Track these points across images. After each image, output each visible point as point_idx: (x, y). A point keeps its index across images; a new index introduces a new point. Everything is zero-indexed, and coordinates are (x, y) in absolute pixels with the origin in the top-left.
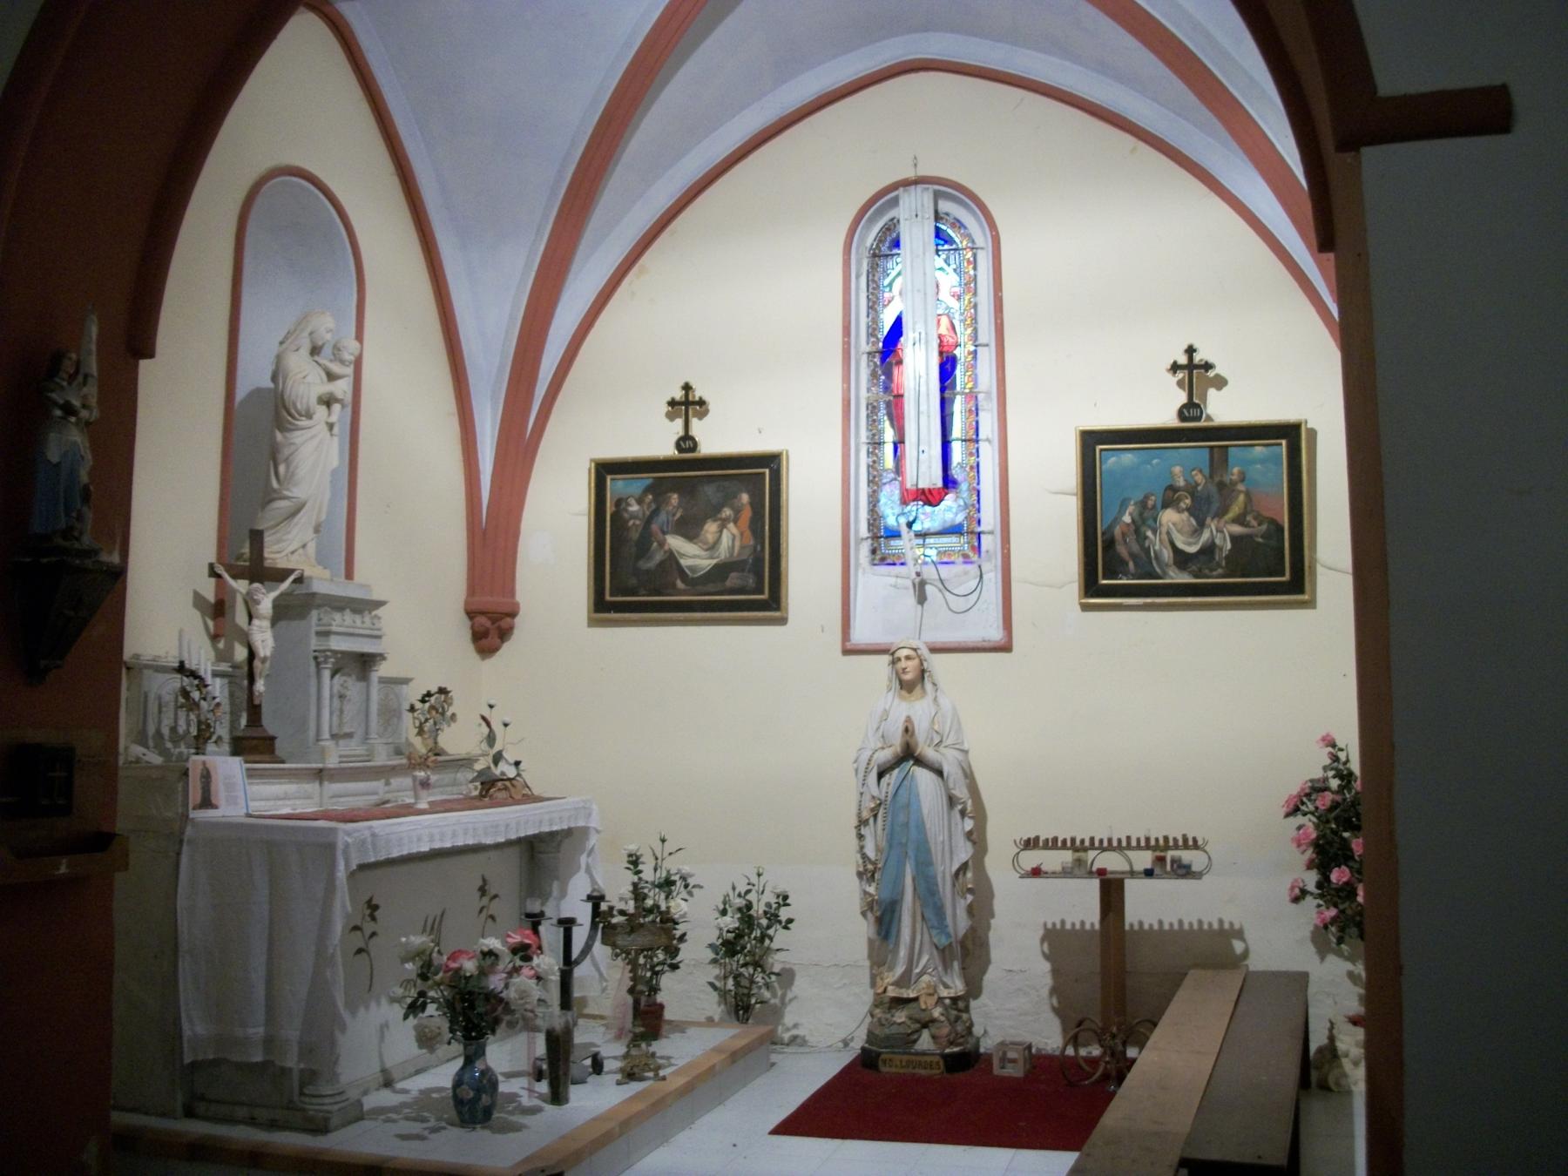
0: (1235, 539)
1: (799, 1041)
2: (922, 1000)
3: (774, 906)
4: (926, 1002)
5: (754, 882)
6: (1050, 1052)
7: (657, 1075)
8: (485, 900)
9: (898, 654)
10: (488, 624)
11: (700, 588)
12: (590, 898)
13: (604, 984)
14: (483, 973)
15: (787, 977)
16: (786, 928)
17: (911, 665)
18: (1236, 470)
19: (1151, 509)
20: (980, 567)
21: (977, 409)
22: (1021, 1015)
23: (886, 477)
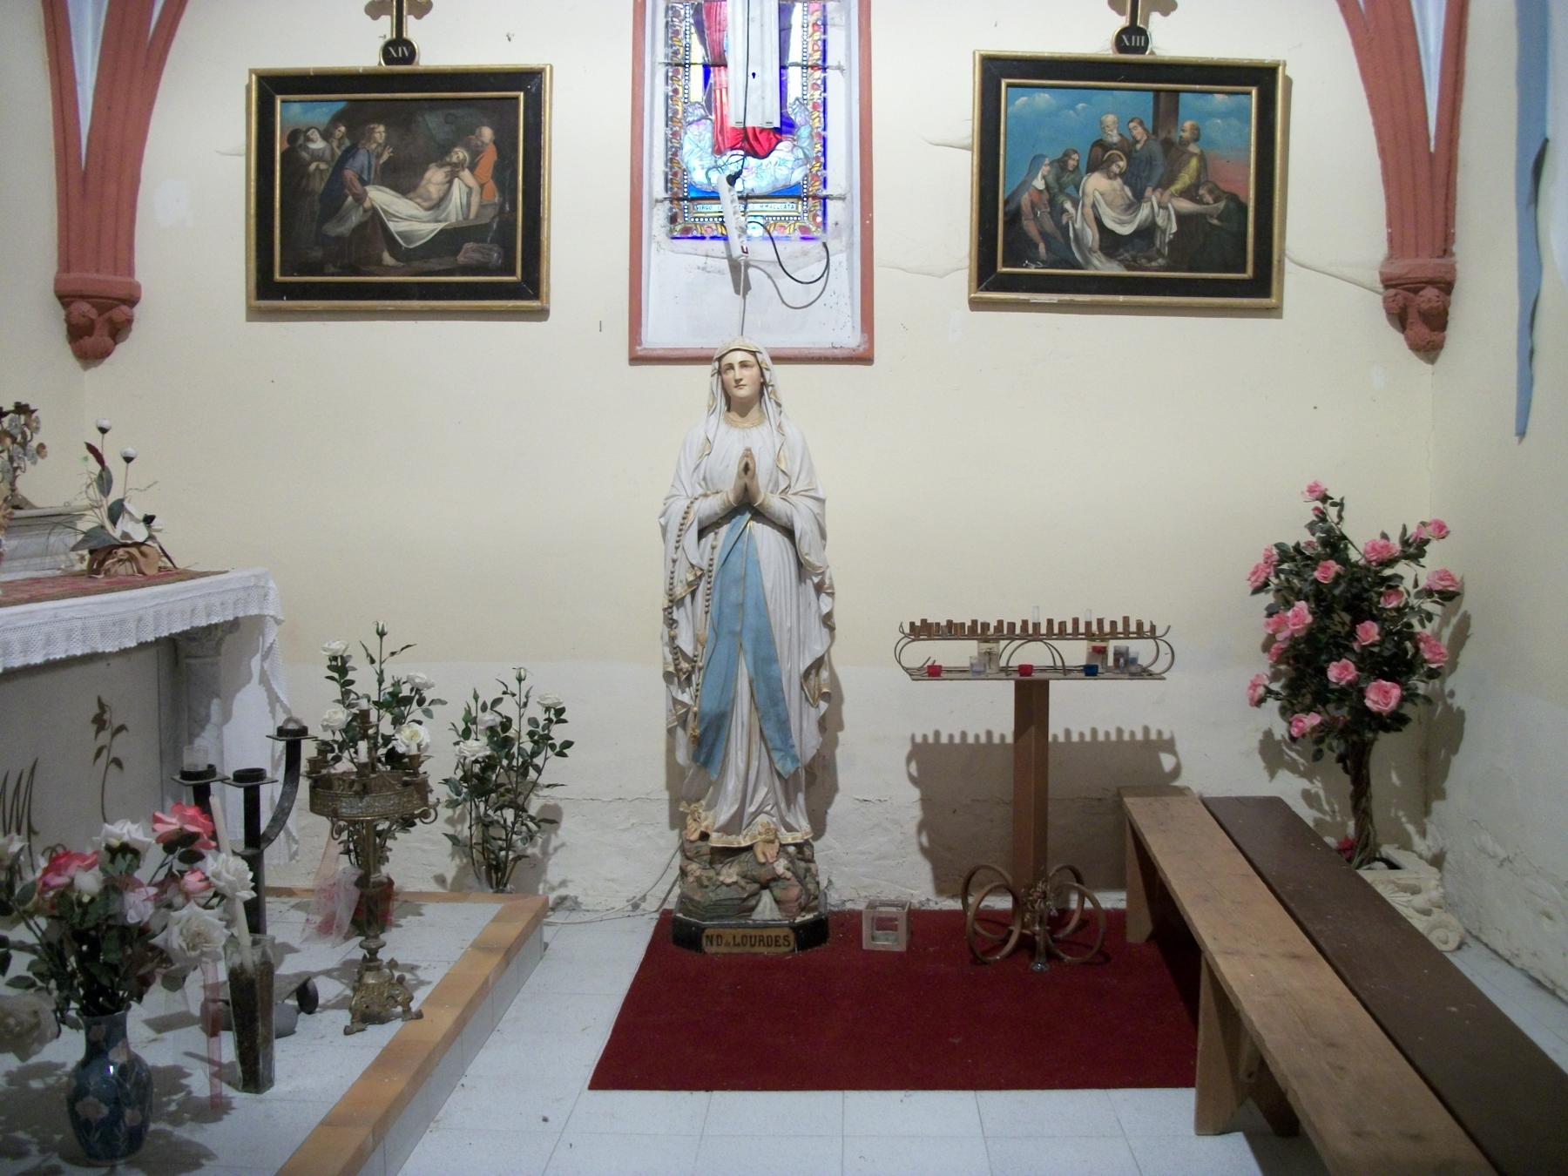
0: (1182, 218)
1: (568, 903)
2: (758, 850)
3: (542, 723)
4: (765, 853)
5: (515, 692)
6: (917, 906)
7: (407, 1010)
8: (105, 737)
9: (726, 360)
10: (93, 314)
11: (416, 264)
12: (281, 732)
13: (295, 847)
14: (114, 888)
15: (550, 820)
16: (561, 754)
17: (749, 376)
18: (1188, 124)
19: (1072, 172)
20: (825, 245)
21: (825, 25)
22: (879, 859)
23: (693, 113)
